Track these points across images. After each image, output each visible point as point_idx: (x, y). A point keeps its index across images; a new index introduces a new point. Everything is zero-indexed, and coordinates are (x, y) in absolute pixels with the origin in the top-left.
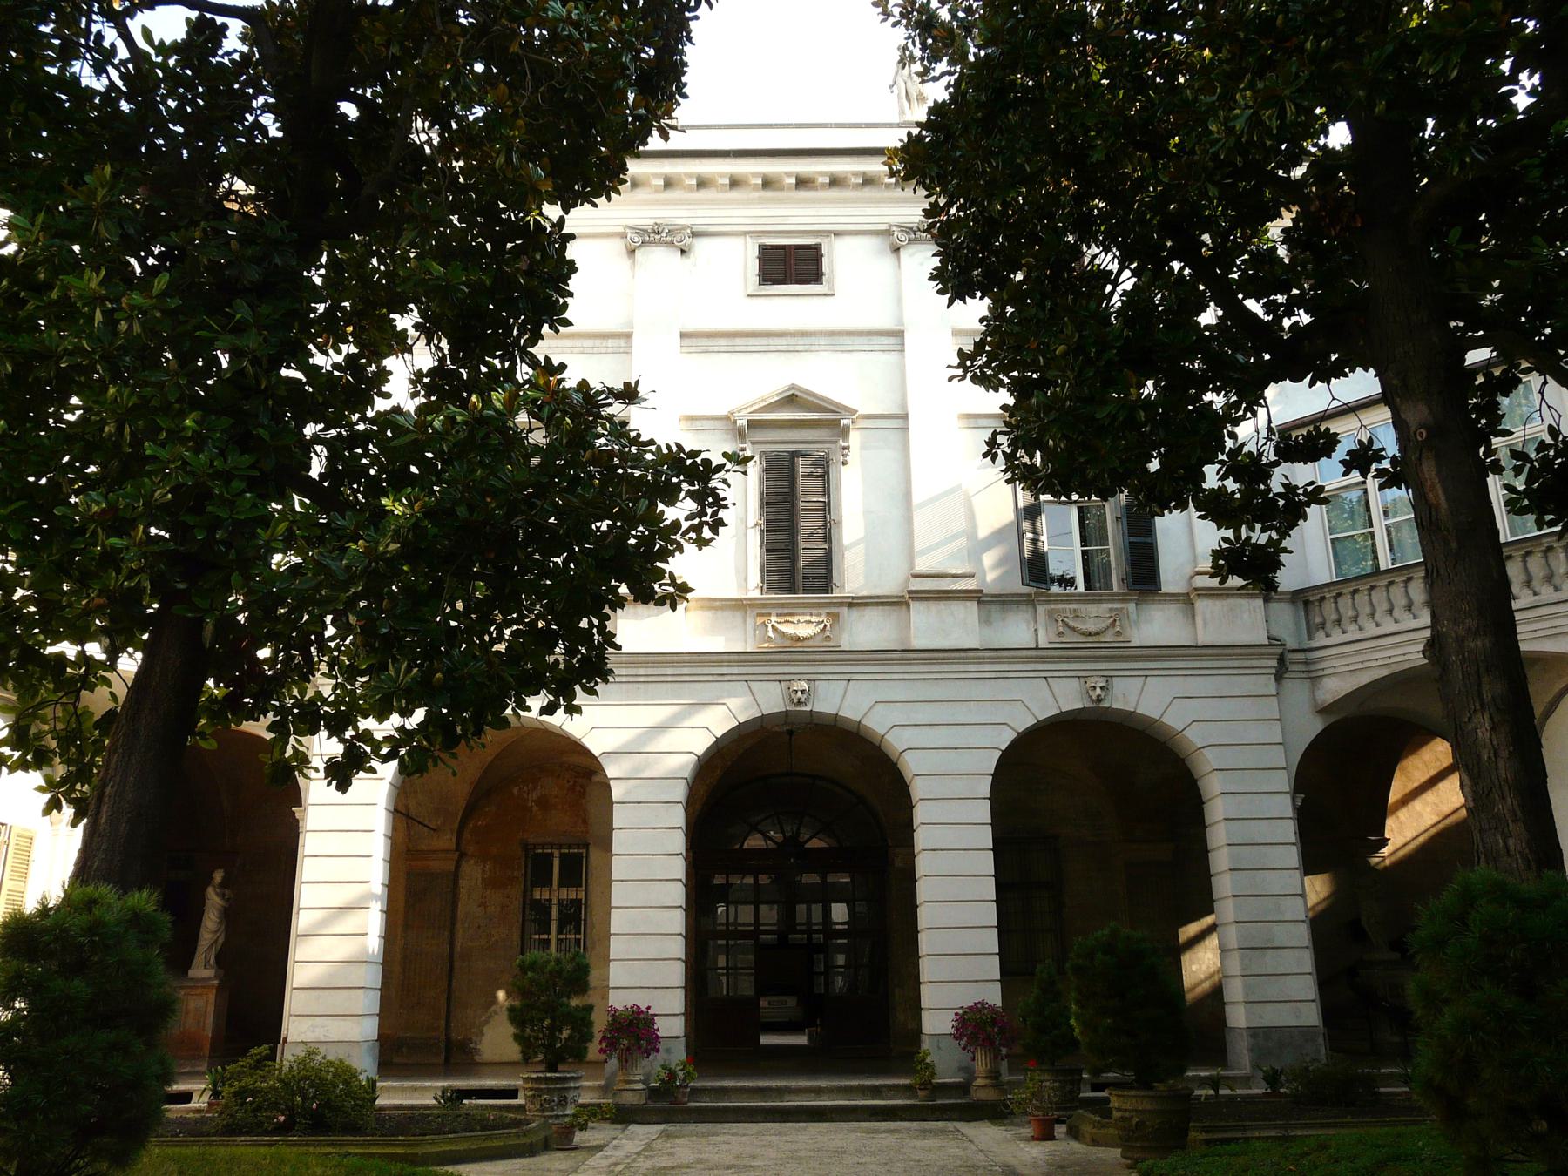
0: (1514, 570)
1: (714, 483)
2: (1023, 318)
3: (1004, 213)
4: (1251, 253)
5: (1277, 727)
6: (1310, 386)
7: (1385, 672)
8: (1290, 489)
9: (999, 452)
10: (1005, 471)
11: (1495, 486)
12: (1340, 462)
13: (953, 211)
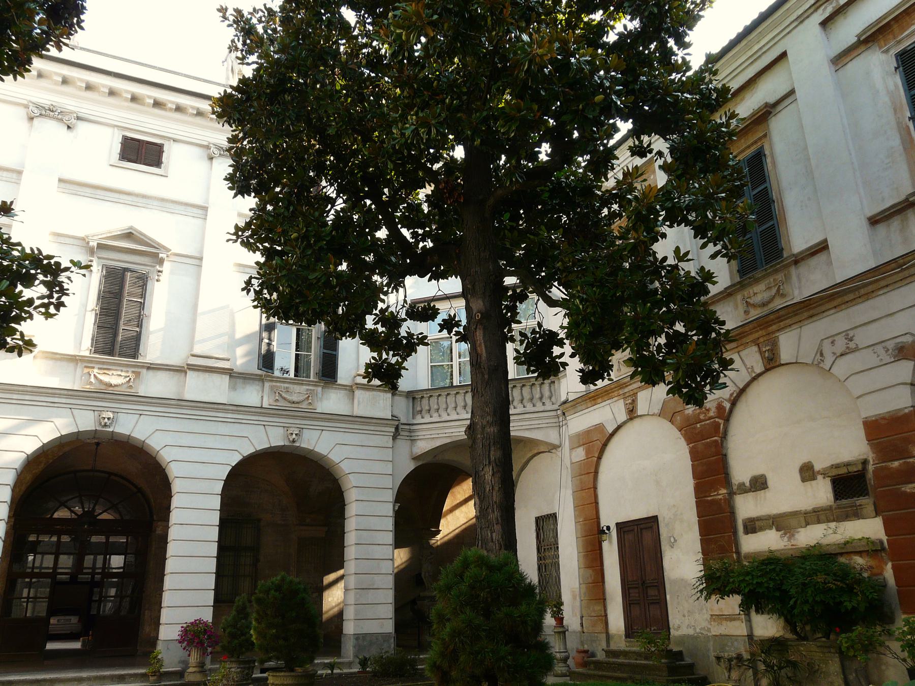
0: (515, 394)
1: (61, 279)
2: (276, 214)
3: (274, 150)
4: (408, 203)
5: (390, 465)
6: (429, 281)
7: (448, 441)
8: (410, 335)
9: (252, 289)
10: (254, 301)
11: (510, 347)
12: (438, 324)
13: (245, 143)
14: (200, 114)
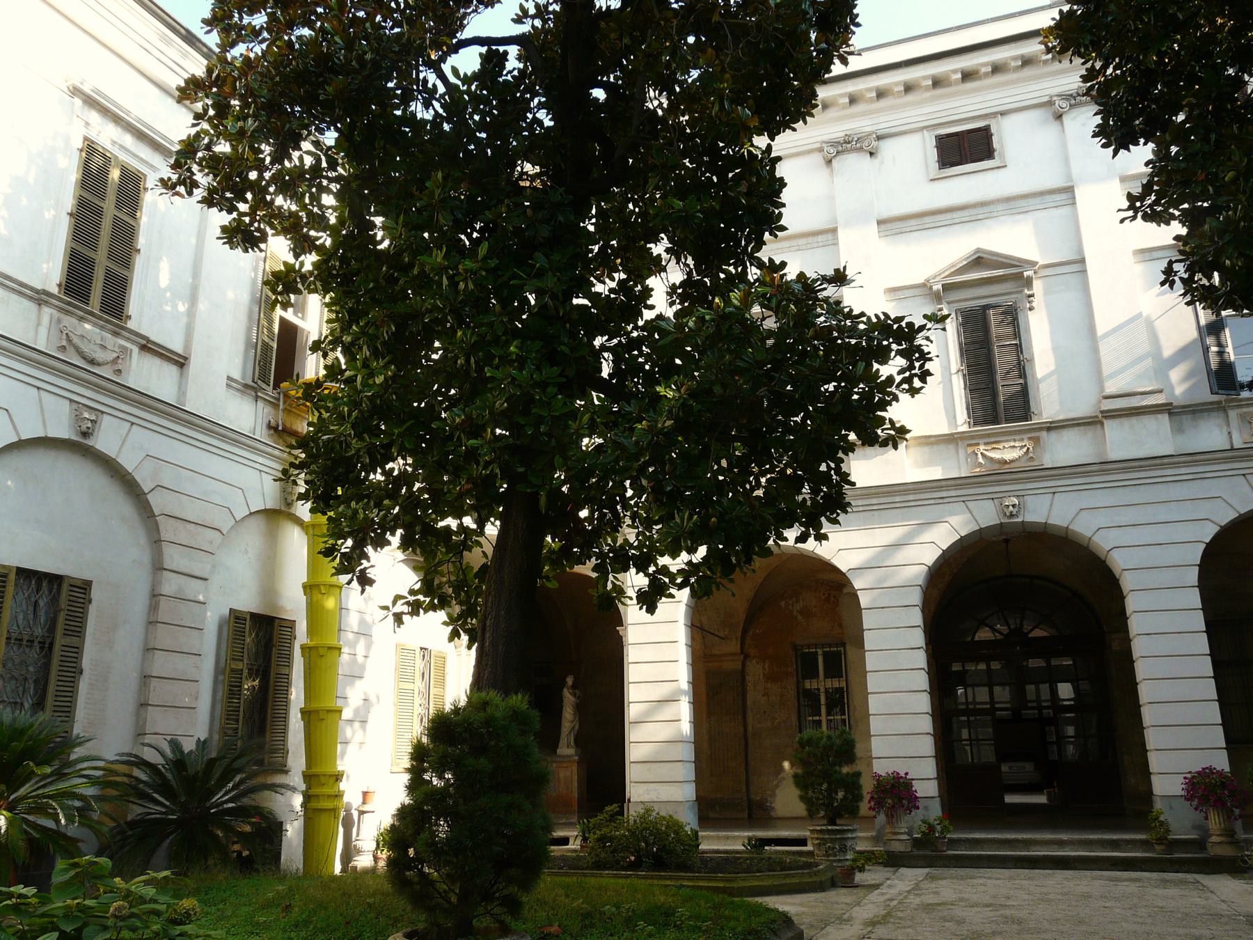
3: (1160, 62)
9: (1176, 278)
10: (1184, 295)
14: (1027, 62)
